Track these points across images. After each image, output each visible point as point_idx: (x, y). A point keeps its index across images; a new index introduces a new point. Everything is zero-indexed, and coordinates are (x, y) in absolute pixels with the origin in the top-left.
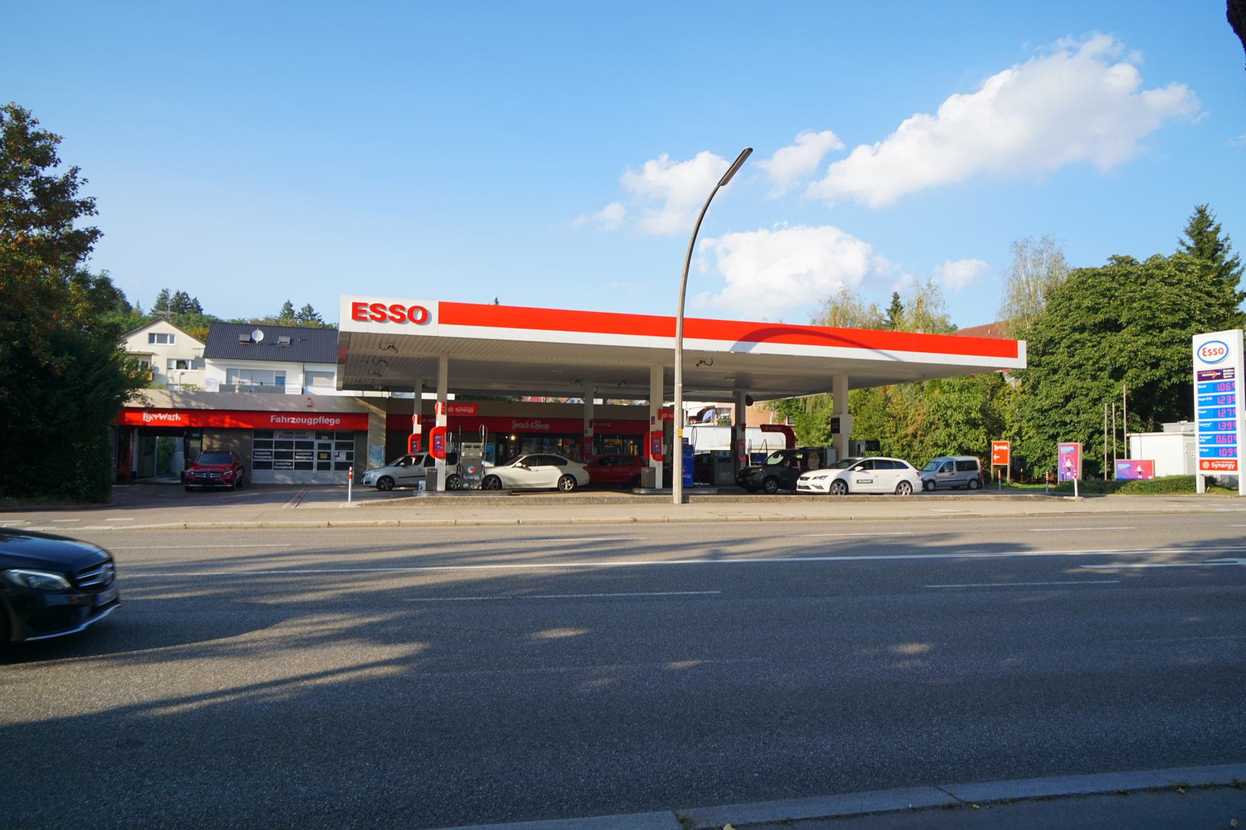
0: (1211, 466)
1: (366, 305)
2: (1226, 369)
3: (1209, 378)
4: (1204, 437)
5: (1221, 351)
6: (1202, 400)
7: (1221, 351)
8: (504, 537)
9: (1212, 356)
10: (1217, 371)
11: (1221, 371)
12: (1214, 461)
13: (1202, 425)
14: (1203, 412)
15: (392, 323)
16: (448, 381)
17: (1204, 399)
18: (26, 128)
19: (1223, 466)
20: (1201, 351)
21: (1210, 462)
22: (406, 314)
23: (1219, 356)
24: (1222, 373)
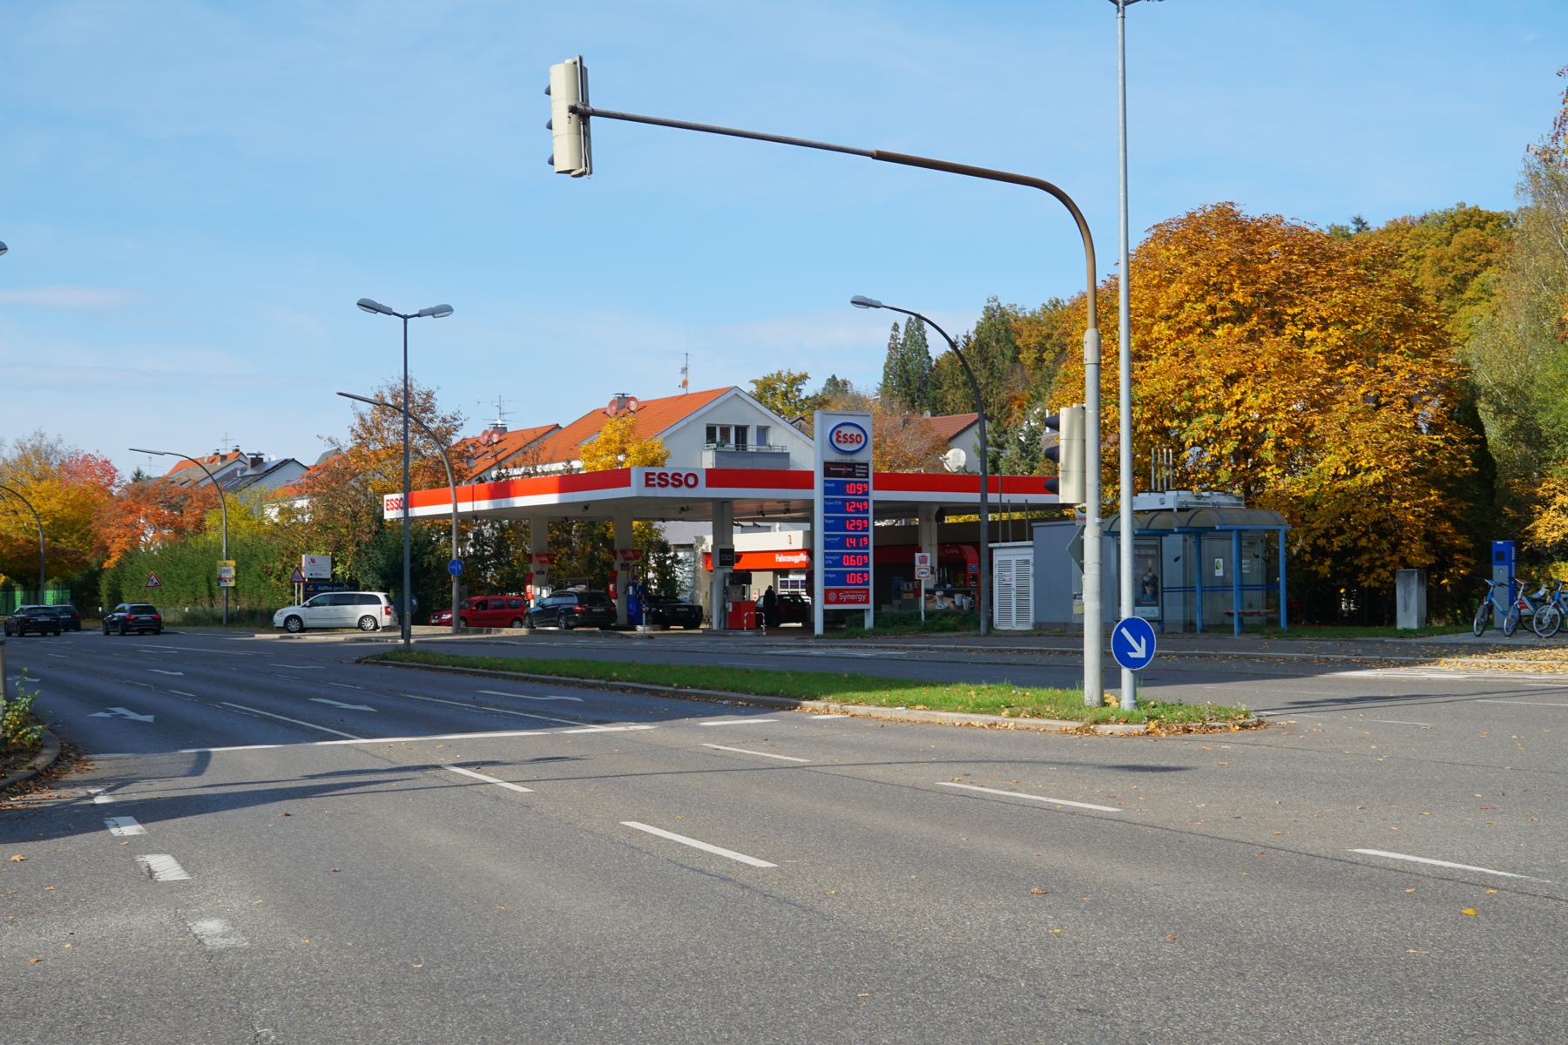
1: (654, 474)
2: (859, 464)
3: (839, 474)
6: (830, 503)
8: (1145, 764)
9: (847, 444)
11: (853, 465)
12: (842, 590)
13: (829, 540)
14: (830, 522)
15: (670, 487)
16: (1083, 630)
18: (1332, 551)
19: (852, 597)
21: (837, 591)
22: (683, 479)
23: (855, 447)
24: (854, 469)
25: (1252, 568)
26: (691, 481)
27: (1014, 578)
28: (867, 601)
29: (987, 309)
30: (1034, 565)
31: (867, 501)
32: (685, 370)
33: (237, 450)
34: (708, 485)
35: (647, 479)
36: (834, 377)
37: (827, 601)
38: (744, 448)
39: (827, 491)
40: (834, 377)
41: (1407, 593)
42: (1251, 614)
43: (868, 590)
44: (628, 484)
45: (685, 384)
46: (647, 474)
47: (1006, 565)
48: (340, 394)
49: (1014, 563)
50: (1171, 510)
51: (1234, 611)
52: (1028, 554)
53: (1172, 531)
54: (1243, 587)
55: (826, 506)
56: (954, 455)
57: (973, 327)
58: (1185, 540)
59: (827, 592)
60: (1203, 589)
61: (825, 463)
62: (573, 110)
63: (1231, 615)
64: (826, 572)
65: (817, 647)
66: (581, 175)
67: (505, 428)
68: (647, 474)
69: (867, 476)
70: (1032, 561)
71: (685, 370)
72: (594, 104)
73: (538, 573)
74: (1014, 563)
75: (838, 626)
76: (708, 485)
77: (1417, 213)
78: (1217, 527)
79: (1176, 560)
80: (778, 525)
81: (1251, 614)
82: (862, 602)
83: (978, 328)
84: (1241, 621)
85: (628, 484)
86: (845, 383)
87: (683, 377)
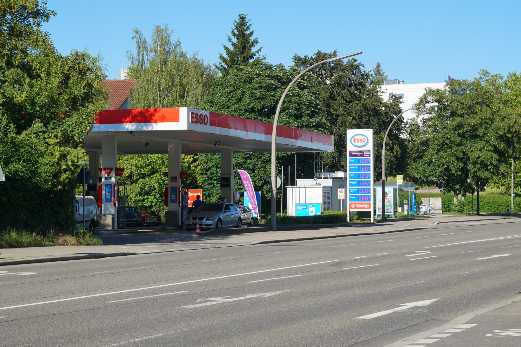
0: (356, 206)
2: (366, 151)
4: (352, 190)
5: (364, 140)
6: (352, 168)
7: (364, 140)
12: (358, 203)
13: (352, 182)
14: (352, 175)
17: (353, 168)
19: (363, 206)
20: (353, 140)
21: (355, 204)
23: (363, 144)
43: (370, 204)
48: (361, 53)
61: (176, 181)
75: (166, 228)
82: (367, 208)
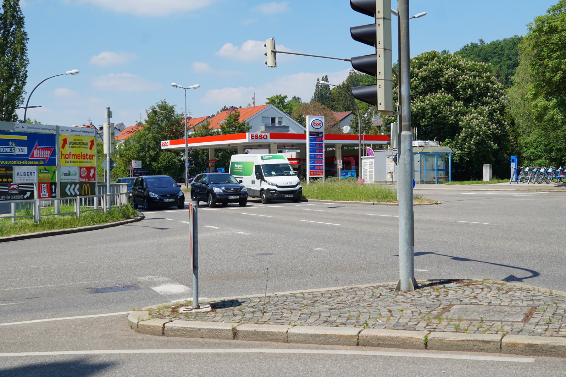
0: (314, 173)
10: (317, 132)
11: (318, 132)
19: (318, 173)
21: (314, 171)
23: (319, 127)
24: (319, 134)
25: (442, 164)
26: (265, 137)
27: (368, 167)
28: (323, 175)
29: (350, 73)
30: (375, 163)
31: (323, 143)
32: (254, 98)
33: (91, 124)
34: (271, 138)
35: (252, 137)
36: (295, 96)
37: (310, 175)
38: (274, 125)
39: (310, 140)
40: (295, 96)
41: (486, 171)
42: (441, 178)
43: (323, 171)
44: (245, 138)
45: (254, 103)
46: (252, 135)
47: (366, 163)
49: (368, 163)
50: (417, 147)
51: (436, 177)
52: (373, 161)
53: (417, 153)
54: (438, 170)
55: (310, 145)
56: (346, 128)
57: (345, 79)
58: (421, 156)
59: (310, 172)
60: (427, 170)
61: (310, 132)
62: (272, 51)
63: (435, 178)
64: (310, 166)
65: (396, 176)
66: (274, 67)
67: (191, 117)
68: (252, 135)
69: (323, 136)
70: (374, 162)
71: (254, 98)
72: (277, 50)
73: (211, 166)
74: (368, 163)
76: (271, 138)
77: (501, 39)
78: (431, 152)
79: (418, 162)
80: (287, 150)
81: (441, 178)
82: (321, 175)
83: (347, 80)
84: (438, 181)
85: (245, 138)
86: (299, 98)
87: (253, 100)
